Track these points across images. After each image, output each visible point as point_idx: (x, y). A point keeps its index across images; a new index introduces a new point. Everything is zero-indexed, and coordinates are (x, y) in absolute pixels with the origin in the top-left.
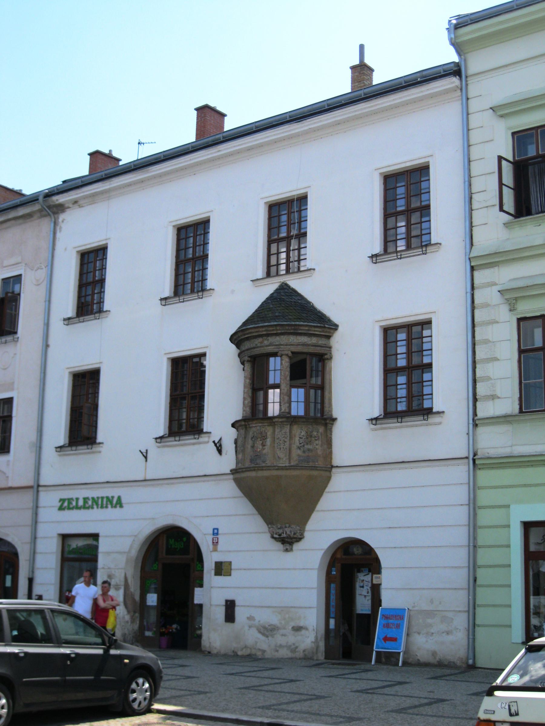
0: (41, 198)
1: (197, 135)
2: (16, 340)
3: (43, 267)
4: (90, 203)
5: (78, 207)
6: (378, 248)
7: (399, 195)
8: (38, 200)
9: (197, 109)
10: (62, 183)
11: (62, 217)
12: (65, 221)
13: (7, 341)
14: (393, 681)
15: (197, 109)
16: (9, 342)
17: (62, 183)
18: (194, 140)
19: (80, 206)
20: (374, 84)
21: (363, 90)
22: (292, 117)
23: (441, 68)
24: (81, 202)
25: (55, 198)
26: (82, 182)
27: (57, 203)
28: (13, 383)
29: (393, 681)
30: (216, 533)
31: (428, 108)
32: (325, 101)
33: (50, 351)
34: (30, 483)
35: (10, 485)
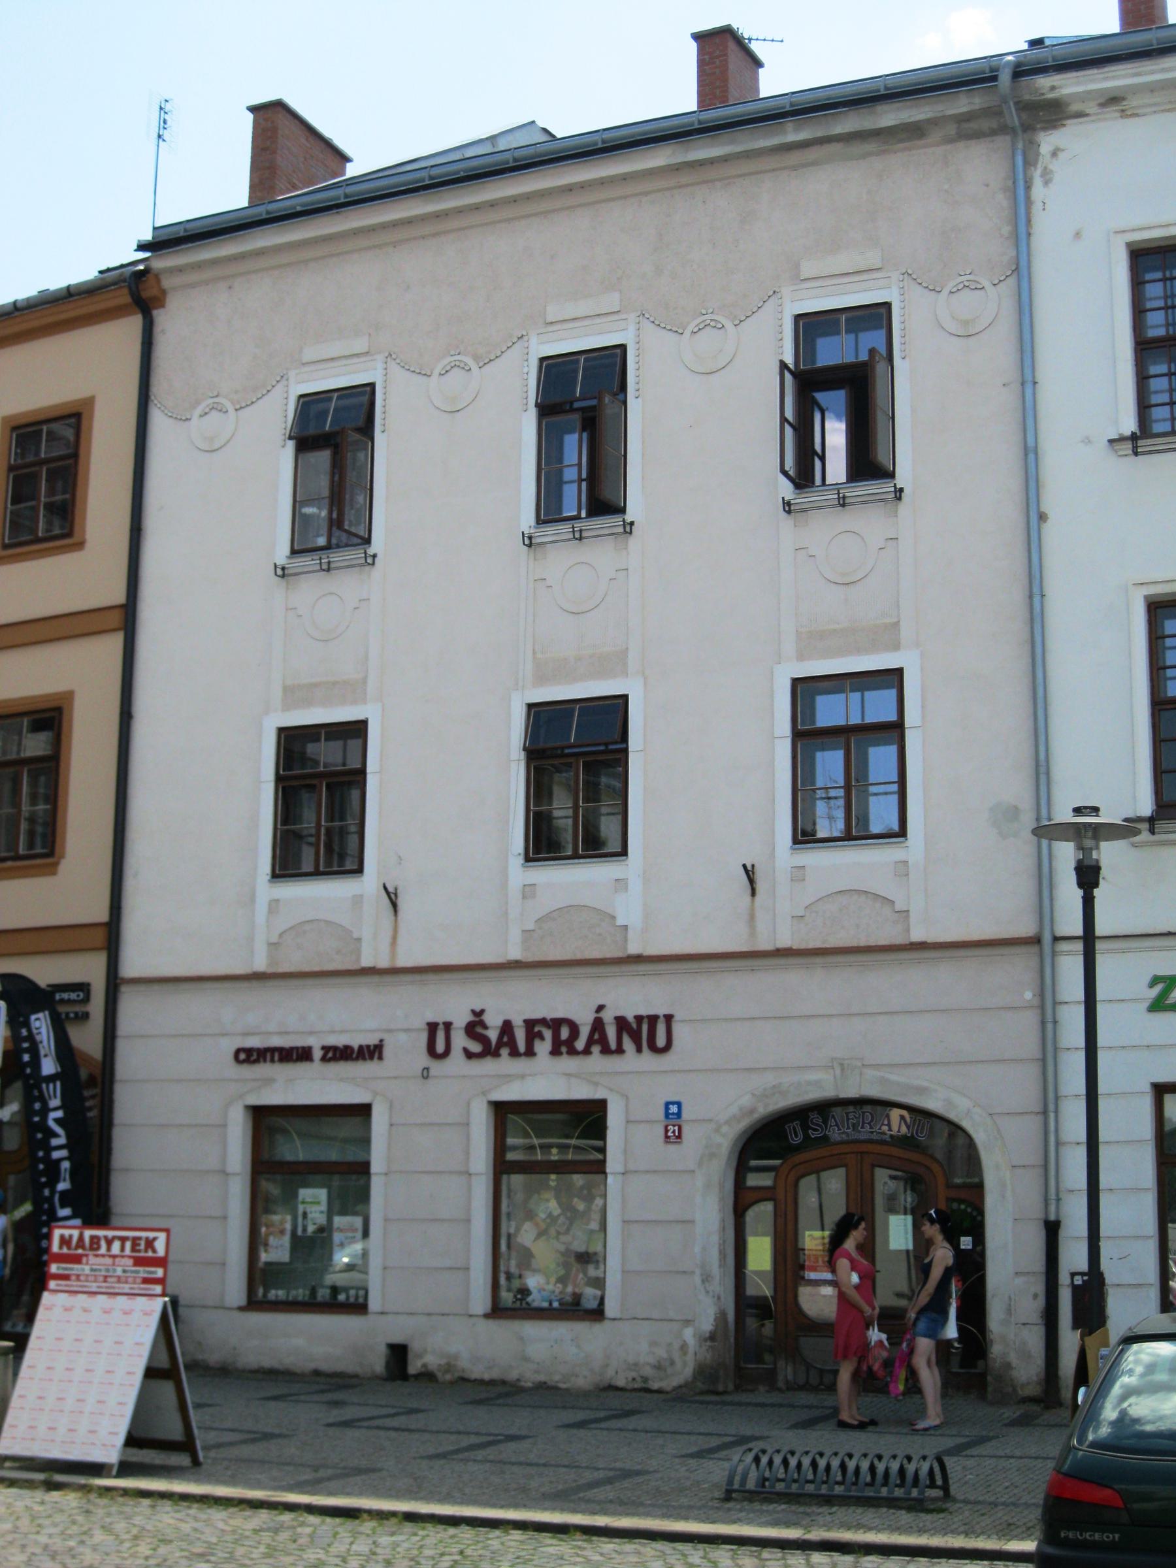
0: (1005, 77)
1: (253, 187)
2: (370, 560)
3: (986, 284)
4: (1168, 107)
5: (1118, 115)
6: (1129, 425)
7: (1151, 299)
8: (994, 78)
9: (698, 37)
10: (1025, 46)
11: (1047, 141)
12: (1061, 155)
13: (332, 565)
14: (241, 1431)
15: (698, 37)
16: (337, 568)
17: (1025, 46)
18: (244, 203)
19: (1124, 114)
20: (761, 96)
21: (343, 188)
22: (350, 197)
23: (508, 156)
24: (1133, 102)
25: (1044, 82)
26: (185, 230)
27: (1050, 96)
28: (896, 625)
29: (241, 1431)
30: (673, 1114)
31: (1155, 112)
32: (787, 94)
33: (1052, 533)
34: (1026, 928)
35: (917, 935)
